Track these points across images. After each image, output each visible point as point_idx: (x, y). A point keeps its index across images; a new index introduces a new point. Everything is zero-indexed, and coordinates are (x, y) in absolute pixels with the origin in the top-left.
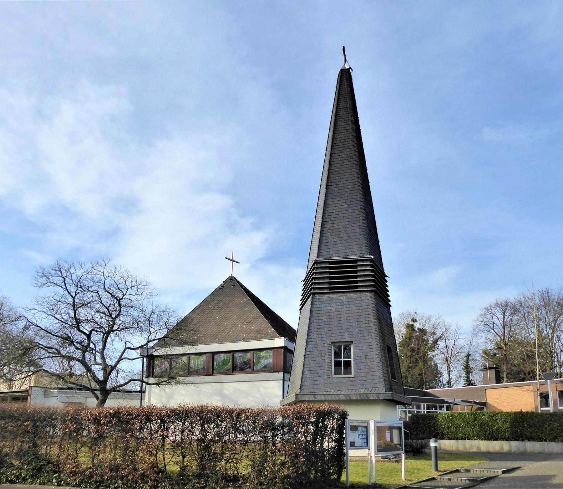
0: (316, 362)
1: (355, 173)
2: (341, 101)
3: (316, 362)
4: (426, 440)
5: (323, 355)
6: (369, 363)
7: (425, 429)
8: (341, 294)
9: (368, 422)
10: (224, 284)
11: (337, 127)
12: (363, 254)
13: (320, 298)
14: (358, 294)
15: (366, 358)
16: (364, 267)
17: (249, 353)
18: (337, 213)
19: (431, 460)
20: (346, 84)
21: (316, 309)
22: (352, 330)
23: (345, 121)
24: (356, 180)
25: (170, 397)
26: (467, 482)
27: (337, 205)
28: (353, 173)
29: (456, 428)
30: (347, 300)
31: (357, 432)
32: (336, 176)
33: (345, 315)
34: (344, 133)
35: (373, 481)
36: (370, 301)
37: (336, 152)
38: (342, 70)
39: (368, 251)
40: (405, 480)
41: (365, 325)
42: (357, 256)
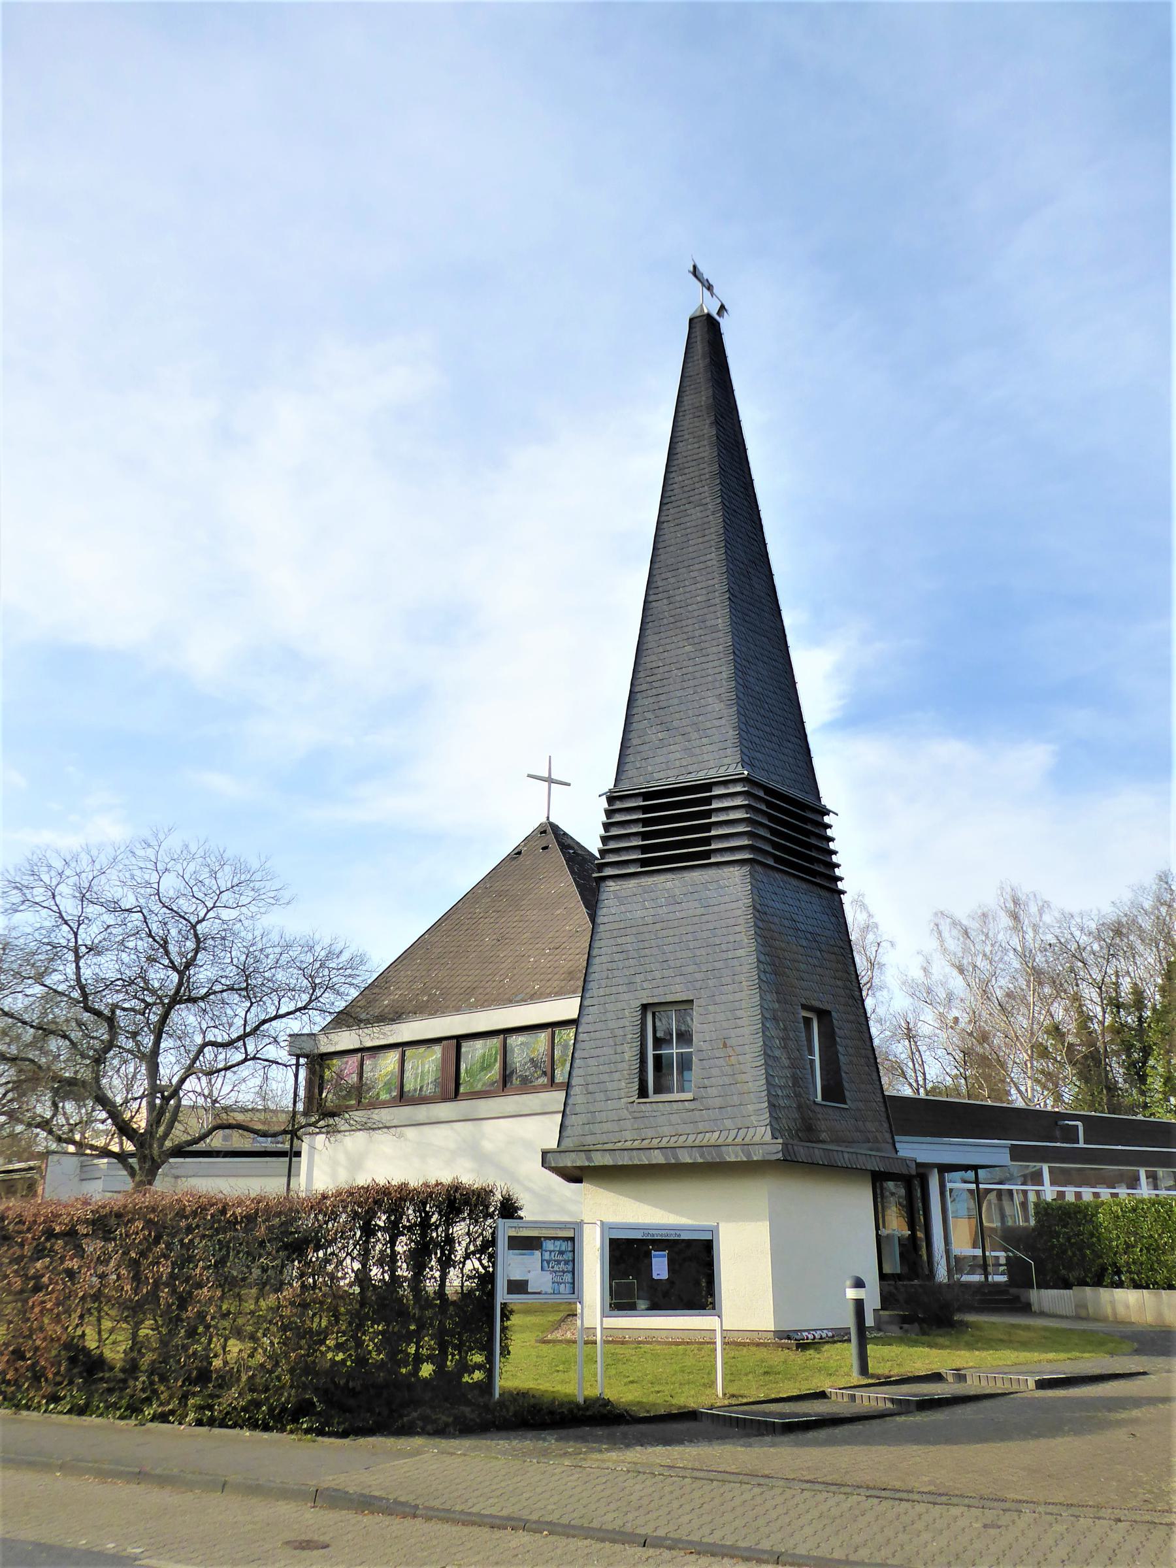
0: (602, 1059)
1: (715, 563)
2: (687, 393)
3: (602, 1059)
4: (1022, 1290)
5: (619, 1040)
6: (733, 1060)
7: (1070, 1253)
8: (669, 876)
9: (578, 1226)
10: (525, 845)
11: (676, 457)
12: (726, 767)
13: (618, 887)
14: (712, 873)
15: (725, 1045)
16: (729, 799)
17: (543, 1035)
18: (667, 668)
19: (849, 1341)
20: (700, 351)
21: (605, 920)
22: (691, 969)
23: (696, 440)
24: (716, 581)
25: (356, 1163)
26: (889, 1405)
27: (668, 648)
28: (709, 563)
29: (1148, 1249)
30: (684, 890)
31: (537, 1253)
32: (669, 575)
33: (677, 931)
34: (691, 469)
35: (593, 1392)
36: (740, 890)
37: (669, 518)
38: (691, 320)
39: (738, 758)
40: (724, 1394)
41: (725, 956)
42: (712, 773)
